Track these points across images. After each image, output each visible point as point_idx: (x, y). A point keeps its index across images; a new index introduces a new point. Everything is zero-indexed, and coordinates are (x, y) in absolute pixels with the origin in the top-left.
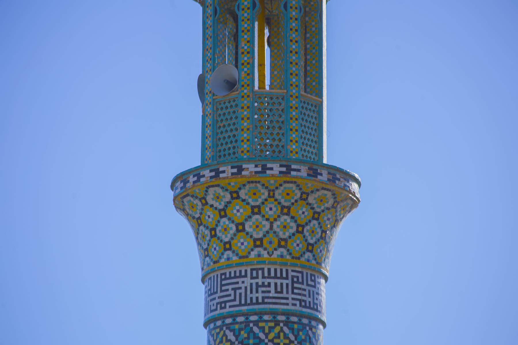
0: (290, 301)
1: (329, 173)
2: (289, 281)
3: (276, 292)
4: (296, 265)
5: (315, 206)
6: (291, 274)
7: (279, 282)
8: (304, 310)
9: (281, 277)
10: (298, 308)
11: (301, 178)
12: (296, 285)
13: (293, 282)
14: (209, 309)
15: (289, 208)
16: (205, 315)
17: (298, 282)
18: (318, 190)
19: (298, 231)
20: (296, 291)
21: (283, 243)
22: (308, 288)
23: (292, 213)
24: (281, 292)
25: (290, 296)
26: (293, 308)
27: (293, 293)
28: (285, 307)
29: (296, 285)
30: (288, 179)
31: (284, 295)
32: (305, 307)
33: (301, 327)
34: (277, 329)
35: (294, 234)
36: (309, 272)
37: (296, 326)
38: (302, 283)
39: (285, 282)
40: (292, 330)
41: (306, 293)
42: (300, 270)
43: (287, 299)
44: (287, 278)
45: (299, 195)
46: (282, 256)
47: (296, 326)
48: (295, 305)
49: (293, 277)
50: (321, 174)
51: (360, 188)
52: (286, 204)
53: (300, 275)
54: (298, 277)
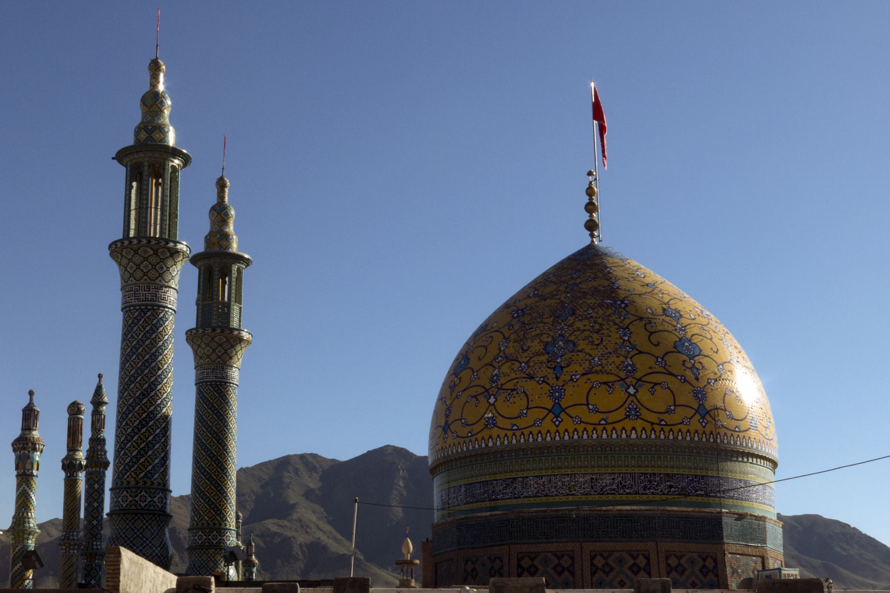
14: (123, 304)
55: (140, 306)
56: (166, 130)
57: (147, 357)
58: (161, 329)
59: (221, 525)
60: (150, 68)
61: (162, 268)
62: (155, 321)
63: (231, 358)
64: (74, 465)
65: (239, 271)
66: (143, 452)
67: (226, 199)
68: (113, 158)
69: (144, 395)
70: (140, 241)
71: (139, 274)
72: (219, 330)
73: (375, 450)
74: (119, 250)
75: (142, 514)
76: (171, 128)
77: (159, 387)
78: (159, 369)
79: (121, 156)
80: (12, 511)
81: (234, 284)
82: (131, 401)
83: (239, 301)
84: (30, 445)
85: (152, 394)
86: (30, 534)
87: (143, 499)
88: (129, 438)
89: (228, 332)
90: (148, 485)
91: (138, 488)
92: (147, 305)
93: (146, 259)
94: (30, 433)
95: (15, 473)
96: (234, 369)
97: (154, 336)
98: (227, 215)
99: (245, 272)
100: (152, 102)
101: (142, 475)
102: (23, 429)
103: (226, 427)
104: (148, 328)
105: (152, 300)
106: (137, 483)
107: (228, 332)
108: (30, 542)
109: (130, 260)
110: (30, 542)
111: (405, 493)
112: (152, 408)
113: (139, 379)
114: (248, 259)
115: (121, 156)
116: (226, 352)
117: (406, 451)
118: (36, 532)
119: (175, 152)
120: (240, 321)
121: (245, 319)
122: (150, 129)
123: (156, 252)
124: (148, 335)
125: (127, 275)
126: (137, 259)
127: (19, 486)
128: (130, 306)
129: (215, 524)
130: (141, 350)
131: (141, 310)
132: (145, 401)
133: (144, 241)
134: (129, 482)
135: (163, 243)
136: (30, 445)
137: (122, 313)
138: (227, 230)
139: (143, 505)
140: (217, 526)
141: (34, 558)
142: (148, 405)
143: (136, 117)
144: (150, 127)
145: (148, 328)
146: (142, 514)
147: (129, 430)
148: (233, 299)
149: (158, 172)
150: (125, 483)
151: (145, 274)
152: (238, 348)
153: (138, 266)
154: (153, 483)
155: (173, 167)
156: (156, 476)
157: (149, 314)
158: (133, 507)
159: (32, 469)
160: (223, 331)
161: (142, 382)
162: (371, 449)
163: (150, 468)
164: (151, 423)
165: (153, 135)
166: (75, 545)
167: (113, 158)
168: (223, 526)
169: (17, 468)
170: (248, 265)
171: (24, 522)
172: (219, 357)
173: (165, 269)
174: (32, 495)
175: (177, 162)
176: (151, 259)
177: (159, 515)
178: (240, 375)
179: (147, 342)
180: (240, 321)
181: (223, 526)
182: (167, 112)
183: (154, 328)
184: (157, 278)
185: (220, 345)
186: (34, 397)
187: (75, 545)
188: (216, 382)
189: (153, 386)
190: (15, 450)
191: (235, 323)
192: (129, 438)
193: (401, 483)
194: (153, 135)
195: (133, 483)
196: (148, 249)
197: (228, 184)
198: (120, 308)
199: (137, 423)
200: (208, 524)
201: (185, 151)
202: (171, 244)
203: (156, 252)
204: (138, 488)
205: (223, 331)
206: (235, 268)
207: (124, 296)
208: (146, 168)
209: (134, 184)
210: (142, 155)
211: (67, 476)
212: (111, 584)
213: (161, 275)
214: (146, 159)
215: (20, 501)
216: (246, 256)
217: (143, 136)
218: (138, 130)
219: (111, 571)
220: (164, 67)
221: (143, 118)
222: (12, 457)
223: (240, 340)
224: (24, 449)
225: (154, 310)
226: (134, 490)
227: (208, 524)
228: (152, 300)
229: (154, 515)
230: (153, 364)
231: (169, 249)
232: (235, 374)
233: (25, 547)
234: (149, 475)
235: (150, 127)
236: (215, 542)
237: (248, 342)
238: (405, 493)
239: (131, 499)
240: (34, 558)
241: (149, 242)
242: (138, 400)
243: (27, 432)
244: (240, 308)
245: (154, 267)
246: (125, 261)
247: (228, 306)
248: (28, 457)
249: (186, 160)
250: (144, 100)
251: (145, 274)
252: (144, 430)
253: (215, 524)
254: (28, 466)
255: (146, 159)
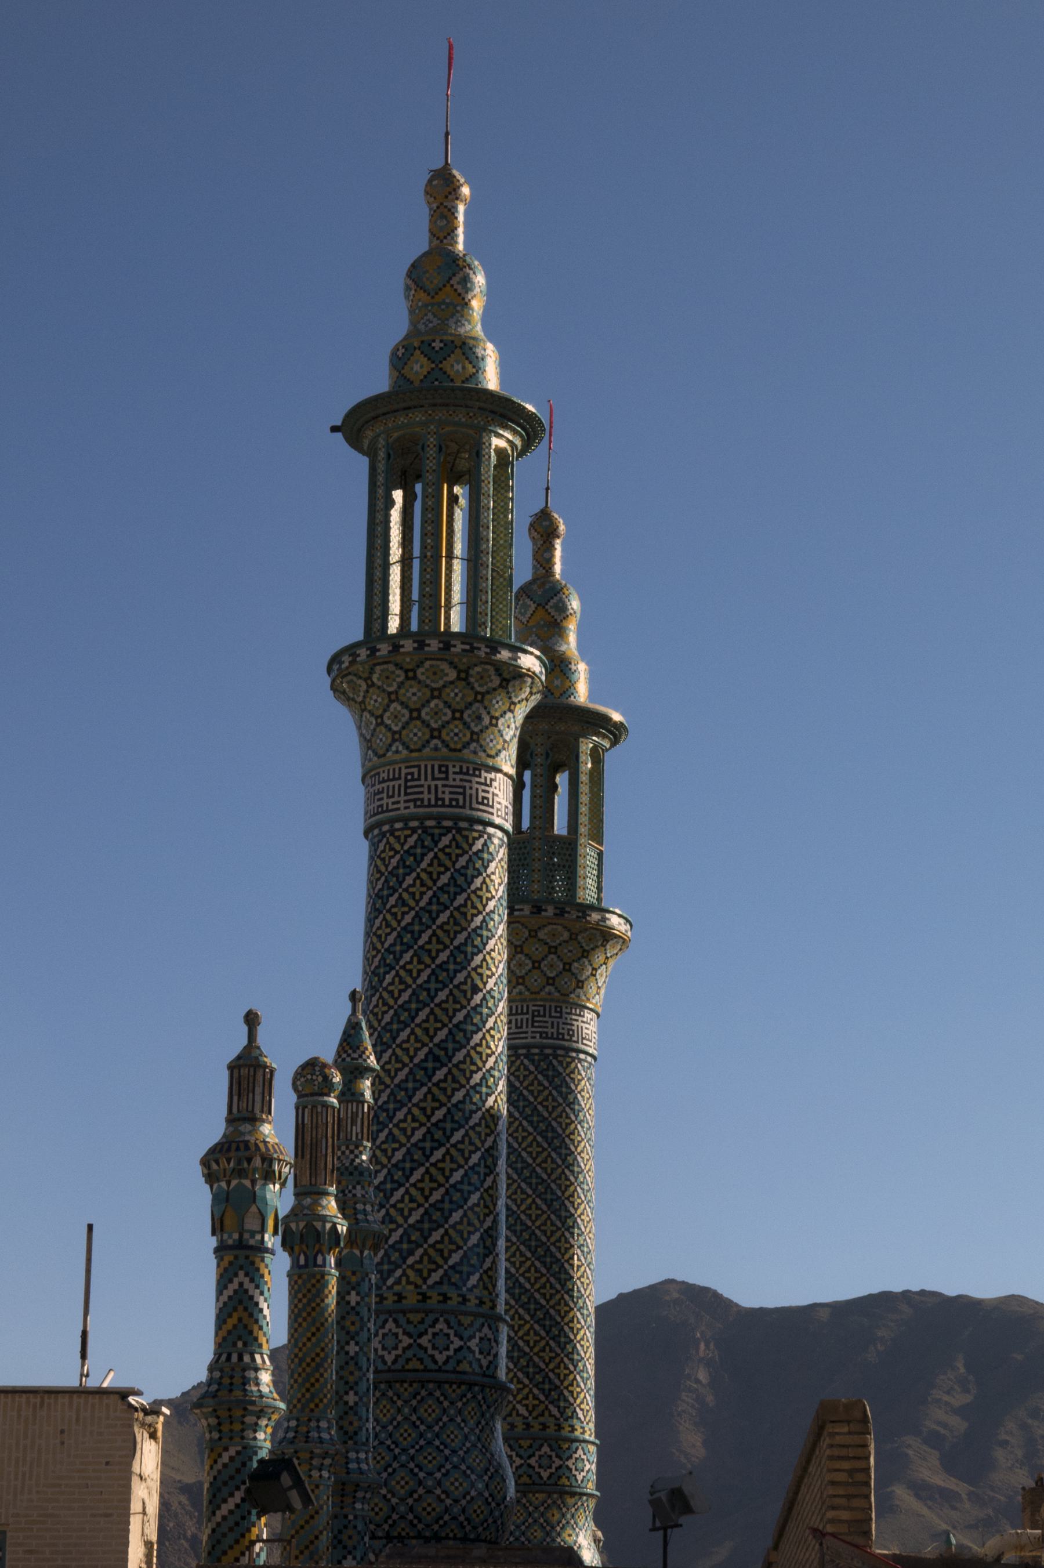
0: (529, 1035)
1: (556, 908)
2: (529, 1016)
3: (517, 1027)
4: (536, 1000)
5: (548, 941)
6: (532, 1008)
7: (519, 1017)
8: (545, 1041)
9: (522, 1013)
10: (538, 1040)
11: (523, 916)
12: (536, 1019)
13: (533, 1016)
14: (369, 814)
15: (521, 946)
16: (366, 820)
17: (539, 1016)
18: (545, 926)
19: (534, 967)
20: (536, 1024)
21: (521, 981)
22: (550, 1020)
23: (526, 951)
24: (521, 1027)
25: (530, 1029)
26: (533, 1040)
27: (533, 1026)
28: (524, 1041)
29: (536, 1019)
30: (375, 661)
31: (524, 1029)
32: (547, 1038)
33: (542, 1057)
34: (518, 1062)
35: (530, 971)
36: (553, 1005)
37: (536, 1057)
38: (544, 1016)
39: (525, 1017)
40: (532, 1061)
41: (549, 1025)
42: (416, 763)
43: (526, 1033)
44: (527, 1013)
45: (527, 933)
46: (520, 993)
47: (536, 1057)
48: (534, 1037)
49: (533, 1011)
50: (546, 910)
51: (1003, 1553)
52: (518, 943)
53: (541, 1009)
54: (539, 1011)
55: (421, 819)
56: (479, 352)
57: (443, 957)
58: (478, 882)
59: (560, 1428)
60: (430, 191)
61: (479, 718)
62: (462, 861)
63: (580, 984)
64: (318, 1235)
65: (597, 756)
66: (437, 1216)
67: (558, 568)
68: (334, 429)
69: (437, 1059)
70: (421, 645)
71: (416, 734)
72: (550, 911)
73: (636, 1293)
74: (364, 670)
75: (440, 1384)
76: (490, 347)
77: (477, 1038)
78: (476, 990)
79: (355, 426)
80: (206, 1352)
81: (584, 789)
82: (402, 1075)
83: (597, 835)
84: (257, 1162)
85: (460, 1056)
86: (261, 1413)
87: (440, 1342)
88: (398, 1175)
89: (574, 914)
90: (453, 1303)
91: (427, 1312)
92: (439, 818)
93: (436, 693)
94: (255, 1130)
95: (213, 1242)
96: (588, 1015)
97: (460, 900)
98: (562, 609)
99: (611, 760)
100: (438, 280)
101: (435, 1277)
102: (231, 1120)
103: (570, 1166)
104: (444, 879)
105: (454, 804)
106: (425, 1297)
107: (574, 914)
108: (261, 1436)
109: (392, 697)
110: (261, 1436)
111: (710, 1399)
112: (459, 1095)
113: (422, 1015)
114: (619, 726)
115: (355, 426)
116: (567, 968)
117: (715, 1295)
118: (277, 1409)
119: (502, 410)
120: (599, 889)
121: (617, 882)
122: (433, 355)
123: (463, 676)
124: (444, 898)
125: (383, 737)
126: (413, 694)
127: (223, 1281)
128: (391, 821)
129: (544, 1427)
130: (425, 937)
131: (425, 830)
132: (440, 1074)
133: (434, 645)
134: (400, 1297)
135: (483, 651)
136: (257, 1162)
137: (364, 846)
138: (563, 648)
139: (441, 1358)
140: (551, 1431)
141: (286, 1480)
142: (449, 1085)
143: (394, 322)
144: (437, 345)
145: (444, 879)
146: (440, 1384)
147: (399, 1155)
148: (583, 830)
149: (462, 463)
150: (391, 1298)
151: (435, 734)
152: (599, 958)
153: (415, 714)
154: (465, 1300)
155: (500, 452)
156: (474, 1280)
157: (445, 840)
158: (414, 1364)
159: (263, 1231)
160: (561, 912)
161: (432, 1025)
162: (627, 1289)
163: (455, 1258)
164: (458, 1136)
165: (446, 365)
166: (325, 1455)
167: (334, 429)
168: (565, 1433)
169: (218, 1227)
170: (615, 742)
171: (245, 1381)
172: (551, 981)
173: (486, 720)
174: (264, 1305)
175: (499, 441)
176: (450, 693)
177: (483, 1387)
178: (600, 1031)
179: (443, 918)
180: (599, 889)
181: (565, 1433)
182: (477, 305)
183: (461, 880)
184: (466, 745)
185: (553, 950)
186: (261, 1031)
187: (325, 1455)
188: (542, 1047)
189: (460, 1036)
190: (211, 1178)
191: (587, 893)
192: (398, 1175)
193: (702, 1375)
194: (446, 365)
195: (412, 1299)
196: (445, 666)
197: (562, 528)
198: (360, 826)
199: (419, 1135)
200: (528, 1426)
201: (530, 407)
202: (505, 655)
203: (463, 676)
204: (427, 1312)
205: (561, 912)
206: (586, 746)
207: (373, 796)
208: (432, 452)
209: (398, 495)
210: (419, 417)
211: (295, 1264)
212: (845, 1515)
213: (476, 737)
214: (425, 426)
215: (231, 1322)
216: (617, 717)
217: (419, 367)
218: (400, 359)
219: (842, 1477)
220: (466, 190)
221: (413, 323)
222: (200, 1199)
223: (606, 936)
224: (241, 1173)
225: (459, 830)
226: (415, 1318)
227: (528, 1426)
228: (454, 804)
229: (471, 1385)
230: (460, 977)
231: (499, 668)
232: (588, 1028)
233: (249, 1450)
234: (455, 1278)
235: (437, 345)
236: (545, 1475)
237: (624, 941)
238: (710, 1399)
239: (406, 1341)
240: (286, 1480)
241: (447, 646)
242: (420, 1074)
243: (246, 1127)
244: (600, 855)
245: (458, 714)
246: (375, 701)
247: (569, 847)
248: (253, 1197)
249: (533, 431)
250: (416, 273)
251: (435, 734)
252: (438, 1154)
253: (544, 1427)
254: (251, 1223)
255: (425, 426)
